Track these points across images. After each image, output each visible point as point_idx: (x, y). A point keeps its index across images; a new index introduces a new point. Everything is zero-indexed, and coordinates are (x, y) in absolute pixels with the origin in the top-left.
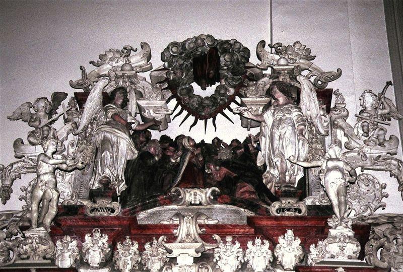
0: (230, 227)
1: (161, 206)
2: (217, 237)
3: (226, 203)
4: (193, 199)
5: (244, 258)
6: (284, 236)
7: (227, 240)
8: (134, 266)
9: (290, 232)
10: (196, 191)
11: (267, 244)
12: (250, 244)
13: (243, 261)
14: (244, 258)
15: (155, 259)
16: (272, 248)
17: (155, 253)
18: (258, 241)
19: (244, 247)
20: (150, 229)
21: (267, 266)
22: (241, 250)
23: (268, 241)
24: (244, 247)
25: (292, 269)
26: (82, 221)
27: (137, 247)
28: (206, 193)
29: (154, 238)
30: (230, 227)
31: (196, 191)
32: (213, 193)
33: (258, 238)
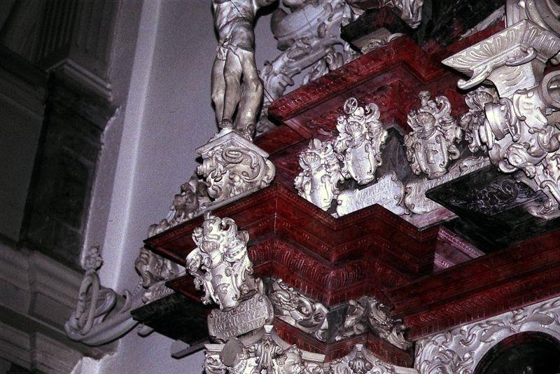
8: (450, 153)
26: (315, 94)
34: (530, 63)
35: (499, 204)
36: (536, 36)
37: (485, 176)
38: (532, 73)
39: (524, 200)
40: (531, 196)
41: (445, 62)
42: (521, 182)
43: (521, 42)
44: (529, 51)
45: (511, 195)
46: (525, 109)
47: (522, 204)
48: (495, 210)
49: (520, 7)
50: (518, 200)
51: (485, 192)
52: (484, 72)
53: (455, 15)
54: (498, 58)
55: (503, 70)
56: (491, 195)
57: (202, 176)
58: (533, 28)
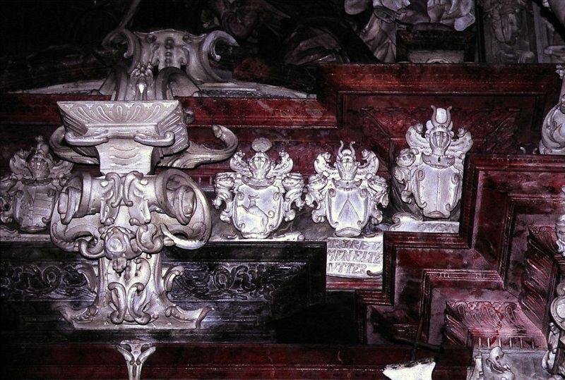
0: (265, 106)
1: (69, 82)
2: (225, 133)
3: (259, 80)
4: (162, 59)
5: (303, 198)
6: (425, 129)
7: (255, 147)
9: (441, 114)
10: (172, 35)
11: (373, 161)
12: (321, 163)
13: (299, 204)
14: (303, 198)
15: (37, 191)
16: (388, 168)
17: (39, 175)
18: (347, 155)
19: (304, 169)
21: (371, 217)
22: (296, 176)
23: (373, 155)
24: (304, 169)
25: (447, 214)
27: (375, 170)
28: (200, 45)
30: (265, 106)
31: (172, 35)
32: (220, 45)
33: (346, 147)
34: (152, 148)
35: (29, 291)
36: (175, 123)
38: (150, 161)
39: (60, 296)
40: (71, 295)
41: (59, 103)
42: (82, 274)
43: (159, 123)
44: (168, 135)
45: (48, 286)
46: (134, 195)
47: (54, 301)
48: (18, 296)
49: (137, 89)
50: (53, 295)
51: (20, 270)
52: (103, 135)
53: (8, 66)
54: (124, 128)
55: (117, 144)
56: (25, 276)
57: (308, 183)
58: (180, 114)
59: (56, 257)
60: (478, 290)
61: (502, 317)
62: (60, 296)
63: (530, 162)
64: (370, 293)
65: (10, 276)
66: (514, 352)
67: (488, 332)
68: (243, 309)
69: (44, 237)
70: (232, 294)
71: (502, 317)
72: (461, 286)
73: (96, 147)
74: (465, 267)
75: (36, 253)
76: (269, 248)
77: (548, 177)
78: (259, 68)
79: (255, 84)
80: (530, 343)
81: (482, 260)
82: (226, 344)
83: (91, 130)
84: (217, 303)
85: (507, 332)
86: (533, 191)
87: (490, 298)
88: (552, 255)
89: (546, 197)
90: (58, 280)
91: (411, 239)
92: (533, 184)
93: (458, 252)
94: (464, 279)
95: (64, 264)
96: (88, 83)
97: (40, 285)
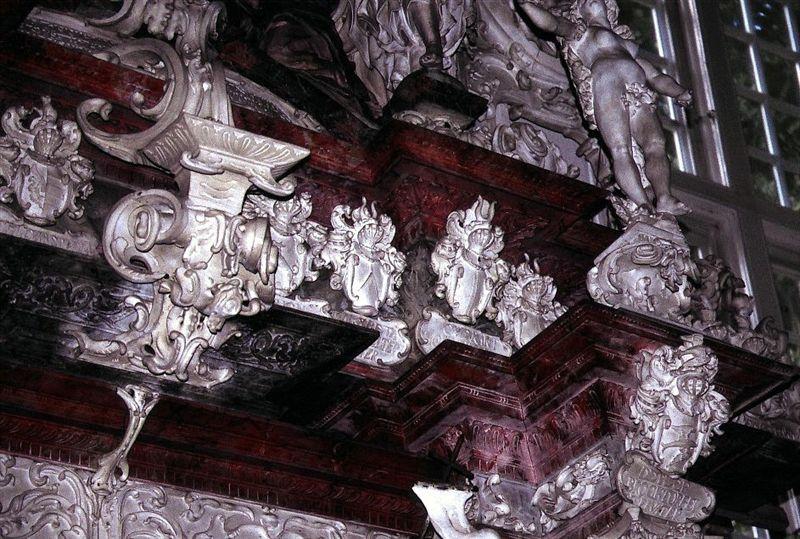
4: (159, 18)
20: (48, 61)
29: (46, 100)
37: (71, 265)
59: (97, 277)
60: (498, 413)
61: (507, 445)
62: (78, 319)
63: (632, 322)
64: (376, 383)
65: (35, 285)
66: (508, 482)
67: (488, 455)
68: (262, 377)
69: (84, 245)
70: (262, 360)
71: (507, 445)
72: (487, 407)
73: (192, 173)
74: (495, 389)
75: (78, 267)
76: (295, 316)
77: (636, 339)
78: (244, 56)
79: (237, 74)
80: (521, 475)
81: (514, 387)
82: (233, 411)
83: (205, 151)
84: (238, 365)
85: (505, 459)
86: (617, 347)
87: (505, 423)
88: (604, 410)
89: (623, 355)
90: (87, 303)
91: (467, 353)
92: (620, 341)
93: (498, 374)
94: (491, 400)
95: (102, 287)
96: (51, 14)
97: (61, 300)
